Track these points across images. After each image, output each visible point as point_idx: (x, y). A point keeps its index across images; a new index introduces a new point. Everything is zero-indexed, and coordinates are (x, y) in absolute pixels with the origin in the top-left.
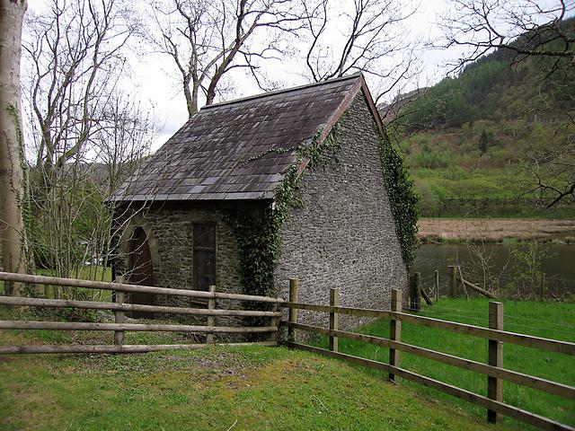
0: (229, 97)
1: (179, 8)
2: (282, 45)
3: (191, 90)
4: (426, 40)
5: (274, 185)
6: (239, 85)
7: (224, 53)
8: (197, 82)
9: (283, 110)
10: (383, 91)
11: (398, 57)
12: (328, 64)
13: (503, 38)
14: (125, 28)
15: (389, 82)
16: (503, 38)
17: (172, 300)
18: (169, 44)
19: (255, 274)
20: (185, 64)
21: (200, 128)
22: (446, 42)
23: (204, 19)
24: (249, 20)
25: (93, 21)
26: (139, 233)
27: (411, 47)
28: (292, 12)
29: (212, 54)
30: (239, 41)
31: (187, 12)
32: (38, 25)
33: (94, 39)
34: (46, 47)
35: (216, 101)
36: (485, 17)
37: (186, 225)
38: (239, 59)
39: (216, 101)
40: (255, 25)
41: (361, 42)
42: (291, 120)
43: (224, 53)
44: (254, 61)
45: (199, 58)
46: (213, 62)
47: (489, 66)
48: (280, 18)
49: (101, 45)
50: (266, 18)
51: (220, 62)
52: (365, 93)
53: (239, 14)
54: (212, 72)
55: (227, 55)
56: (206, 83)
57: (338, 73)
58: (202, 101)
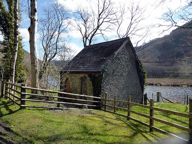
0: (96, 43)
1: (82, 17)
2: (111, 27)
3: (85, 41)
4: (152, 25)
5: (102, 68)
6: (99, 39)
7: (94, 30)
8: (87, 38)
9: (107, 47)
10: (136, 41)
11: (145, 30)
12: (123, 34)
13: (176, 23)
14: (67, 23)
15: (142, 37)
16: (176, 23)
17: (75, 97)
18: (79, 27)
19: (97, 91)
20: (83, 33)
21: (85, 52)
22: (158, 26)
23: (89, 20)
24: (101, 21)
25: (60, 32)
26: (67, 79)
27: (148, 27)
28: (113, 18)
29: (91, 30)
30: (98, 27)
31: (84, 18)
32: (43, 22)
33: (59, 26)
34: (46, 28)
35: (92, 44)
36: (171, 17)
37: (79, 78)
38: (98, 31)
39: (92, 44)
40: (103, 22)
41: (133, 26)
42: (108, 50)
43: (94, 30)
44: (103, 32)
45: (87, 31)
46: (91, 33)
47: (184, 30)
48: (110, 20)
49: (61, 28)
50: (106, 20)
51: (93, 33)
52: (130, 44)
53: (98, 19)
54: (91, 35)
55: (95, 31)
56: (89, 38)
57: (126, 35)
58: (88, 44)
